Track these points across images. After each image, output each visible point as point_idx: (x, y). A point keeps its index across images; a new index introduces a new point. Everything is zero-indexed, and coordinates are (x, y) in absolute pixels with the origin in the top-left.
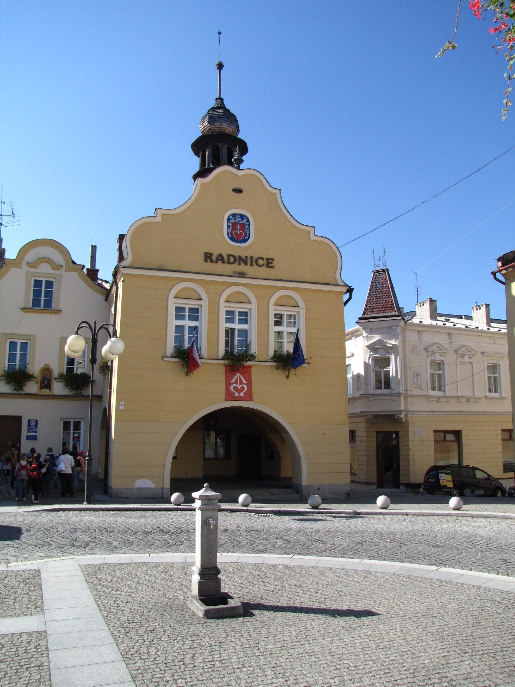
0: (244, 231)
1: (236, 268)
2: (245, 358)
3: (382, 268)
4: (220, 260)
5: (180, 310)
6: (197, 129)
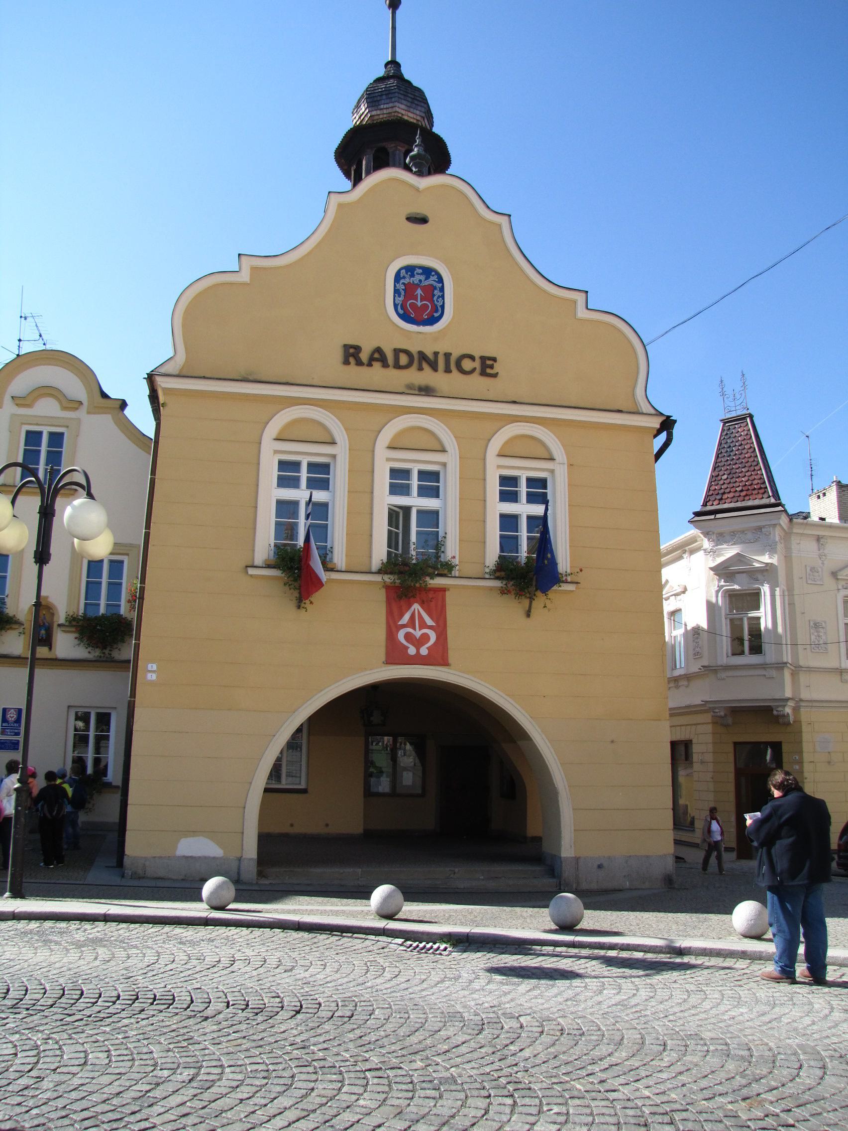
0: (432, 302)
2: (430, 570)
3: (739, 413)
4: (377, 360)
5: (288, 468)
6: (346, 115)
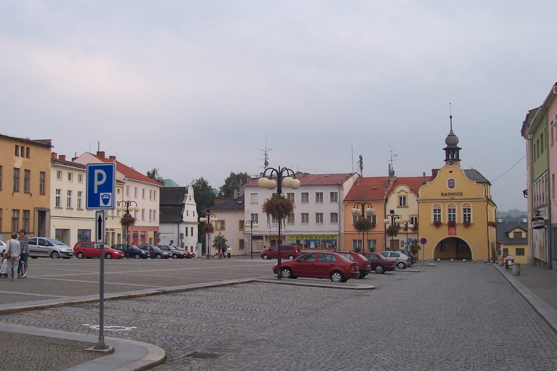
1: (451, 196)
